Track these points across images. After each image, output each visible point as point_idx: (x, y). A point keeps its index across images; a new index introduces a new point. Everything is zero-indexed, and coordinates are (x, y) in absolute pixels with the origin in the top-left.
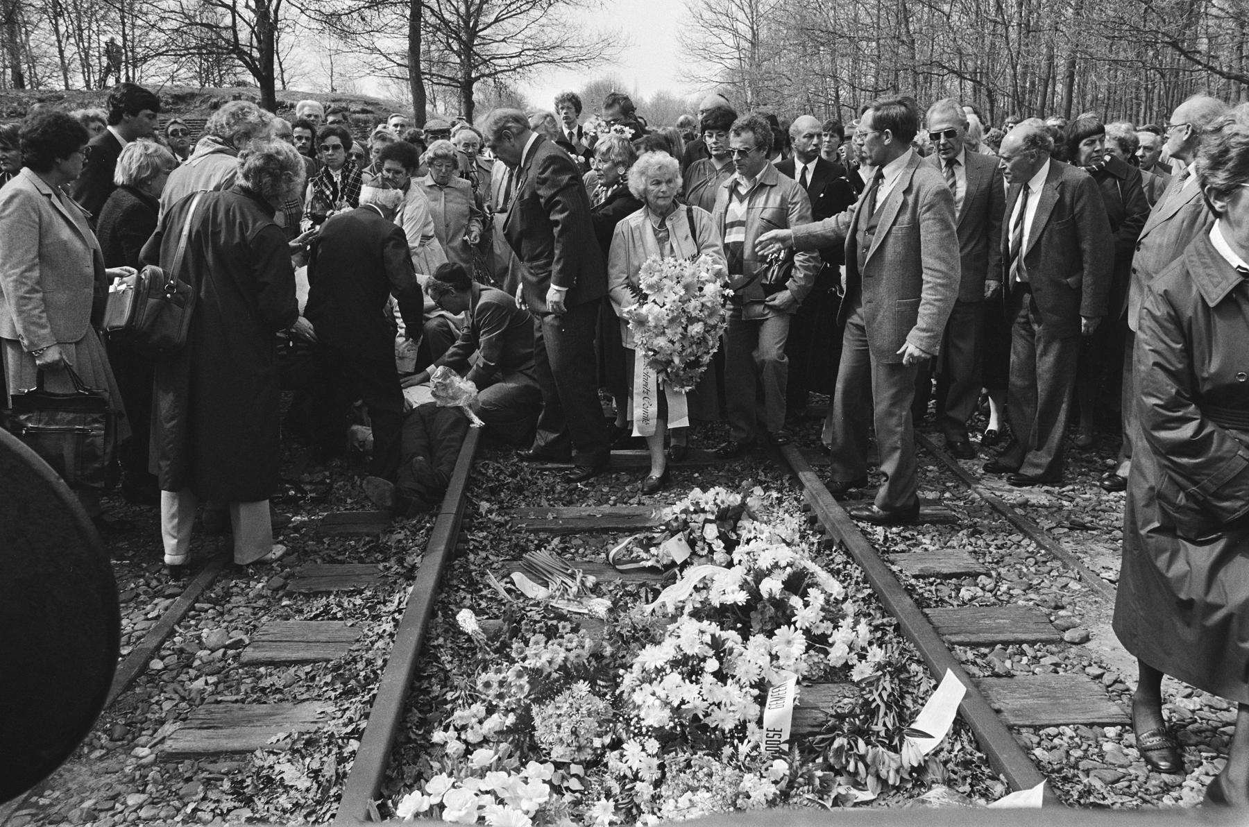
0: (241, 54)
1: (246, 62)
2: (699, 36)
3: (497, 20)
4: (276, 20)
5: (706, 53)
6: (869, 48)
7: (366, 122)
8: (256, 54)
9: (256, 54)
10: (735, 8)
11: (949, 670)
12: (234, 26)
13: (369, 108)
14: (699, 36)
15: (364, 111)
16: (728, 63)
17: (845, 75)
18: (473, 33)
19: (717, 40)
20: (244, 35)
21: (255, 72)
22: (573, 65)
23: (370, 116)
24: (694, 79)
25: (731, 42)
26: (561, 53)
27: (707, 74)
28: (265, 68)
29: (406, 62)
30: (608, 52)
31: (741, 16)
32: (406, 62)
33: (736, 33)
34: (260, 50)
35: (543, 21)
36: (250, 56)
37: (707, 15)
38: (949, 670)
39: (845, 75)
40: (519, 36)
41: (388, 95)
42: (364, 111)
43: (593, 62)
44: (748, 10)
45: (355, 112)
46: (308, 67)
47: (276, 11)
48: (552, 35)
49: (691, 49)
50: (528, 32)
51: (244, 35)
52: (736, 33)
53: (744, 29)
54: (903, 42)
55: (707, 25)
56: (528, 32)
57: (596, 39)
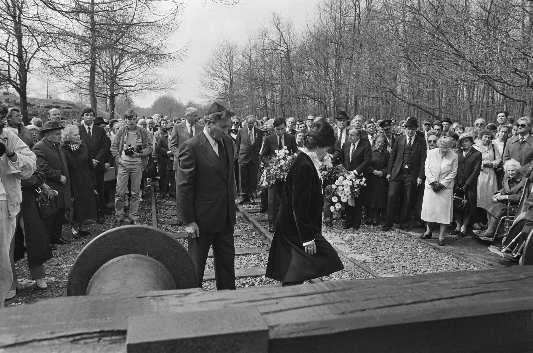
0: (11, 82)
1: (13, 85)
2: (209, 80)
3: (125, 71)
4: (28, 67)
5: (211, 86)
6: (278, 87)
7: (69, 113)
8: (18, 82)
9: (18, 82)
10: (223, 69)
11: (106, 179)
12: (9, 71)
13: (70, 107)
14: (209, 80)
15: (68, 108)
16: (221, 91)
17: (268, 97)
18: (115, 76)
19: (216, 82)
20: (14, 74)
21: (17, 89)
22: (158, 91)
23: (71, 110)
24: (207, 97)
25: (222, 82)
26: (154, 86)
27: (212, 95)
28: (22, 88)
29: (88, 88)
30: (173, 86)
31: (226, 72)
32: (88, 88)
33: (224, 80)
34: (20, 80)
35: (146, 72)
36: (15, 82)
37: (212, 71)
38: (106, 179)
39: (268, 97)
40: (136, 78)
41: (70, 99)
42: (68, 108)
43: (167, 90)
44: (229, 70)
45: (63, 108)
46: (37, 87)
47: (28, 64)
48: (150, 78)
49: (205, 85)
50: (139, 77)
51: (14, 74)
52: (224, 80)
53: (227, 77)
54: (292, 86)
55: (212, 75)
56: (139, 77)
57: (168, 80)
